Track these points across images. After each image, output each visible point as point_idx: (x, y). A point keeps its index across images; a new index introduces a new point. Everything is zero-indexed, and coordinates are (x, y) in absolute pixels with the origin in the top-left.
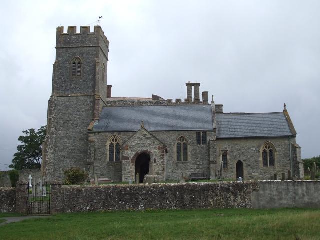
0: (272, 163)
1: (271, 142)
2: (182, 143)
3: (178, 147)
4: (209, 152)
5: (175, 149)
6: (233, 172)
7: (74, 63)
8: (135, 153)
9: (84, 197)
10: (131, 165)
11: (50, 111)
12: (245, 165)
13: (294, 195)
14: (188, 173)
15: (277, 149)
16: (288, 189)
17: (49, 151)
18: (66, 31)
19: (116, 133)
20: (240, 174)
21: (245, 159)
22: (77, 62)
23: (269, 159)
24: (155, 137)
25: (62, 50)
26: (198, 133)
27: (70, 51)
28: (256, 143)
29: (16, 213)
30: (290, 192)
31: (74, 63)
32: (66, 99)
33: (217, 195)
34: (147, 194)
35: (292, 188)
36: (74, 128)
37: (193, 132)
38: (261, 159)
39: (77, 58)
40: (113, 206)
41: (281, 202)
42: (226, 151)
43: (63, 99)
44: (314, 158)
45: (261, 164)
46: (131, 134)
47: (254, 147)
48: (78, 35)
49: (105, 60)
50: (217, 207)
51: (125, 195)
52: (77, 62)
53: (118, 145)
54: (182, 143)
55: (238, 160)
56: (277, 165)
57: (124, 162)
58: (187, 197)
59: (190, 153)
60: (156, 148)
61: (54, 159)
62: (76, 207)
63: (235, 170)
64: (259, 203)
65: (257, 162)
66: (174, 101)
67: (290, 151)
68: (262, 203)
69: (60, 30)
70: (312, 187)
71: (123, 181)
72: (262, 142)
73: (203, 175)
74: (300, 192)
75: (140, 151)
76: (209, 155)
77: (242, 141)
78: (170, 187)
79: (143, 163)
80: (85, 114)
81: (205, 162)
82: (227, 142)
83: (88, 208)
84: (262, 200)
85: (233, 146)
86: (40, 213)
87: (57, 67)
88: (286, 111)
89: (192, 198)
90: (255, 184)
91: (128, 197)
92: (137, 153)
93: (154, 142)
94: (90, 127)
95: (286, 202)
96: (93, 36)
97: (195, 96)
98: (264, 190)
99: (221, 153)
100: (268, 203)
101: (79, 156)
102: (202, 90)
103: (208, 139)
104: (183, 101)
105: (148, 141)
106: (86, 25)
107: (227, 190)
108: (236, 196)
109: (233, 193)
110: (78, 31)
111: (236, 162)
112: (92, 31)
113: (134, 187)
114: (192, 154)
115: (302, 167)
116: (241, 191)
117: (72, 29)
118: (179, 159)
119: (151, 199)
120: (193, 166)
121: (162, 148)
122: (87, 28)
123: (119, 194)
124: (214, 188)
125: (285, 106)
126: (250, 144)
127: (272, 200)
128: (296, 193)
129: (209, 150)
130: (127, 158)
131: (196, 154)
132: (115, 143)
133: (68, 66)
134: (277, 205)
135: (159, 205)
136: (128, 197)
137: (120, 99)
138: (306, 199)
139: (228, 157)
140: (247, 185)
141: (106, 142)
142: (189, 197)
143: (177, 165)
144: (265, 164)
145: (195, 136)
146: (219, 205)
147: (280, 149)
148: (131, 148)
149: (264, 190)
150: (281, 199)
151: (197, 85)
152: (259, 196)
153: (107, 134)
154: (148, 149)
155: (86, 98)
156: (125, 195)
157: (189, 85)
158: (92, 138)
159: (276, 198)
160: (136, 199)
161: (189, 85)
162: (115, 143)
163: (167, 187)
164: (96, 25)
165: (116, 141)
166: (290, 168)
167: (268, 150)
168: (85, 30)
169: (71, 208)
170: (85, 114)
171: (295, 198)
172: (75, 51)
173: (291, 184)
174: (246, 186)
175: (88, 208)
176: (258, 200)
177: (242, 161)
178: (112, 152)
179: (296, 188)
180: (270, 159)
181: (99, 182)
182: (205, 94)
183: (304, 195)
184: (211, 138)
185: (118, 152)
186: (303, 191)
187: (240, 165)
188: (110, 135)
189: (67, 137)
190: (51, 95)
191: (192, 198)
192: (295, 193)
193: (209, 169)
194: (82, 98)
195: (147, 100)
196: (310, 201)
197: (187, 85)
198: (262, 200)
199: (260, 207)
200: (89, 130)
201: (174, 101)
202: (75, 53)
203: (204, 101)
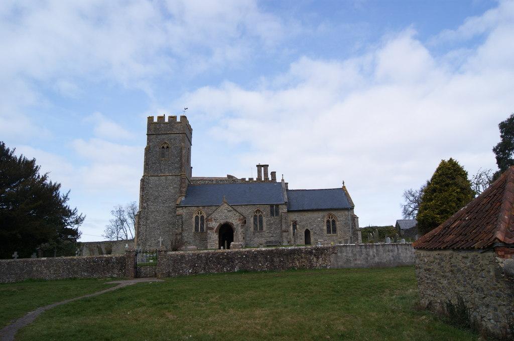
0: (335, 231)
1: (333, 213)
2: (258, 215)
3: (254, 219)
4: (281, 222)
5: (252, 220)
6: (302, 239)
7: (163, 148)
8: (219, 224)
9: (186, 261)
10: (215, 234)
11: (143, 188)
12: (312, 233)
13: (366, 256)
14: (263, 240)
15: (339, 219)
16: (361, 251)
17: (142, 223)
18: (155, 120)
19: (200, 207)
20: (308, 241)
21: (311, 228)
22: (165, 146)
23: (332, 227)
24: (235, 210)
25: (152, 137)
26: (272, 206)
27: (159, 137)
28: (321, 214)
29: (125, 277)
30: (362, 254)
31: (163, 148)
32: (156, 178)
33: (302, 258)
34: (242, 257)
35: (365, 250)
36: (164, 203)
37: (267, 206)
38: (325, 228)
39: (165, 143)
40: (213, 269)
41: (356, 262)
42: (296, 221)
43: (153, 178)
44: (369, 227)
45: (325, 232)
46: (214, 208)
47: (319, 218)
48: (166, 123)
49: (189, 144)
50: (302, 268)
51: (223, 259)
52: (165, 146)
53: (202, 217)
54: (258, 215)
55: (306, 229)
56: (339, 232)
57: (209, 231)
58: (276, 260)
59: (264, 224)
60: (236, 219)
61: (146, 231)
62: (180, 270)
63: (303, 237)
64: (337, 264)
65: (322, 230)
66: (247, 180)
67: (349, 220)
68: (340, 264)
69: (150, 119)
70: (381, 249)
71: (209, 248)
72: (326, 213)
73: (276, 242)
74: (371, 253)
75: (222, 222)
76: (281, 225)
77: (309, 213)
78: (262, 251)
79: (226, 233)
80: (173, 191)
81: (278, 231)
82: (296, 214)
83: (190, 271)
84: (340, 261)
85: (301, 217)
86: (146, 277)
87: (148, 151)
88: (344, 187)
89: (281, 261)
90: (334, 248)
91: (225, 260)
92: (233, 224)
93: (235, 214)
94: (178, 202)
95: (359, 262)
96: (180, 124)
97: (56, 188)
98: (341, 252)
99: (292, 223)
100: (345, 263)
101: (169, 227)
102: (270, 170)
103: (281, 211)
104: (255, 179)
105: (230, 214)
106: (173, 115)
107: (310, 253)
108: (318, 258)
109: (315, 255)
110: (167, 120)
111: (304, 230)
112: (178, 120)
113: (231, 252)
114: (267, 225)
115: (359, 233)
116: (322, 254)
117: (161, 118)
118: (255, 229)
119: (245, 262)
120: (267, 234)
121: (242, 220)
122: (175, 118)
123: (218, 258)
124: (300, 251)
125: (343, 183)
126: (316, 215)
127: (348, 261)
128: (368, 255)
129: (281, 221)
130: (211, 229)
131: (271, 224)
132: (199, 216)
133: (158, 149)
134: (352, 265)
135: (252, 267)
136: (225, 260)
137: (200, 179)
138: (377, 259)
139: (297, 226)
140: (327, 249)
141: (192, 215)
142: (278, 259)
143: (254, 234)
144: (329, 232)
145: (268, 209)
146: (304, 266)
147: (341, 217)
148: (215, 220)
149: (341, 252)
150: (356, 260)
151: (266, 166)
152: (337, 257)
153: (193, 208)
154: (230, 221)
155: (174, 177)
156: (223, 259)
157: (259, 166)
158: (180, 211)
159: (351, 259)
160: (233, 262)
161: (259, 166)
162: (199, 216)
163: (259, 251)
164: (182, 115)
165: (201, 213)
166: (350, 234)
167: (331, 220)
168: (172, 119)
169: (175, 272)
170: (173, 191)
171: (367, 259)
172: (164, 137)
173: (363, 247)
174: (326, 249)
175: (190, 271)
176: (337, 261)
177: (309, 229)
178: (197, 223)
179: (368, 250)
180: (333, 228)
181: (190, 250)
182: (273, 174)
183: (374, 256)
184: (283, 209)
185: (202, 224)
186: (374, 252)
187: (307, 233)
188: (195, 209)
189: (157, 211)
190: (143, 175)
191: (281, 261)
192: (367, 254)
193: (281, 237)
194: (171, 177)
195: (205, 179)
196: (380, 261)
197: (257, 166)
198: (340, 261)
199: (338, 267)
200: (177, 205)
201: (247, 180)
202: (164, 139)
203: (272, 180)
